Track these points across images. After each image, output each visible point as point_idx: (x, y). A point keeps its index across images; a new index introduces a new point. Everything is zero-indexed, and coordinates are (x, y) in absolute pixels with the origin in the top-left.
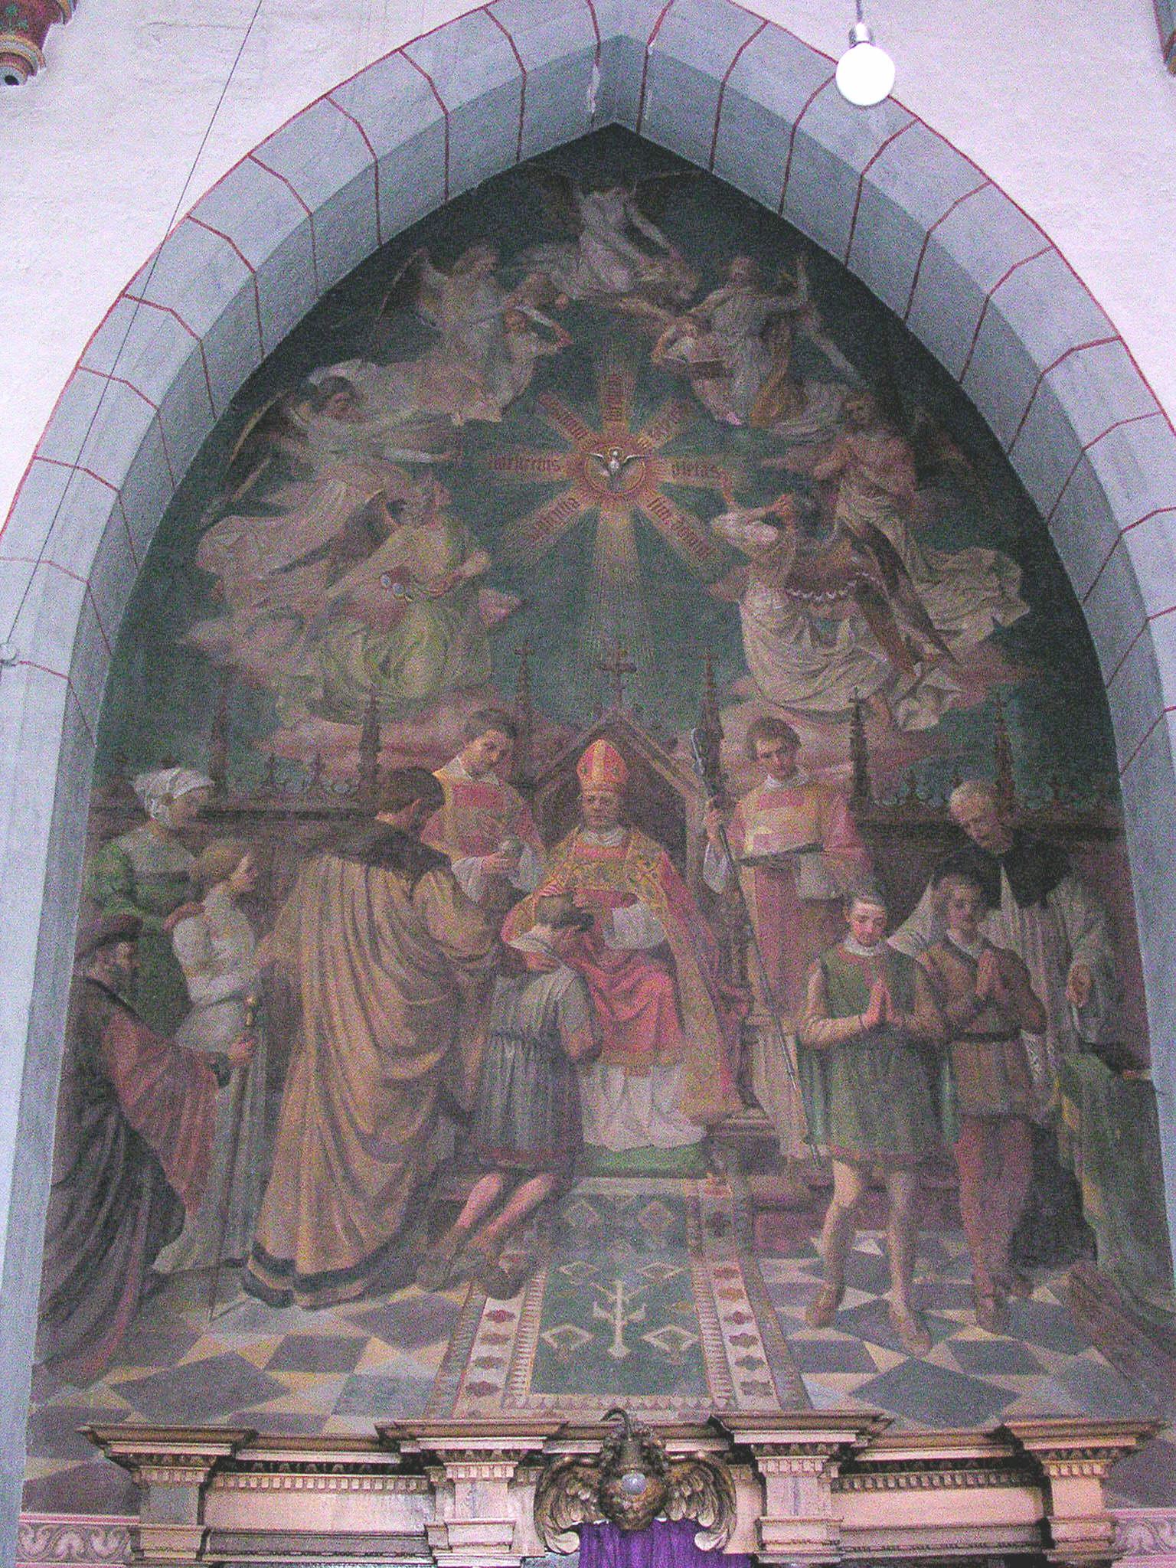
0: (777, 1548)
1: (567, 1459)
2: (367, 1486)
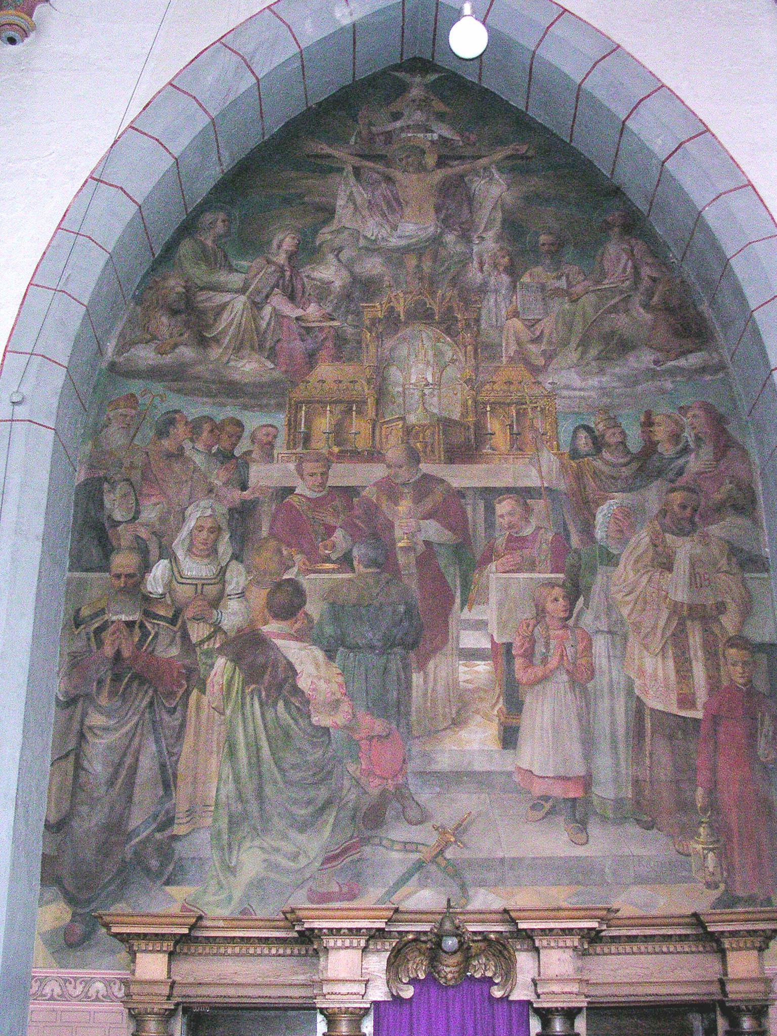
1: (411, 937)
2: (266, 951)
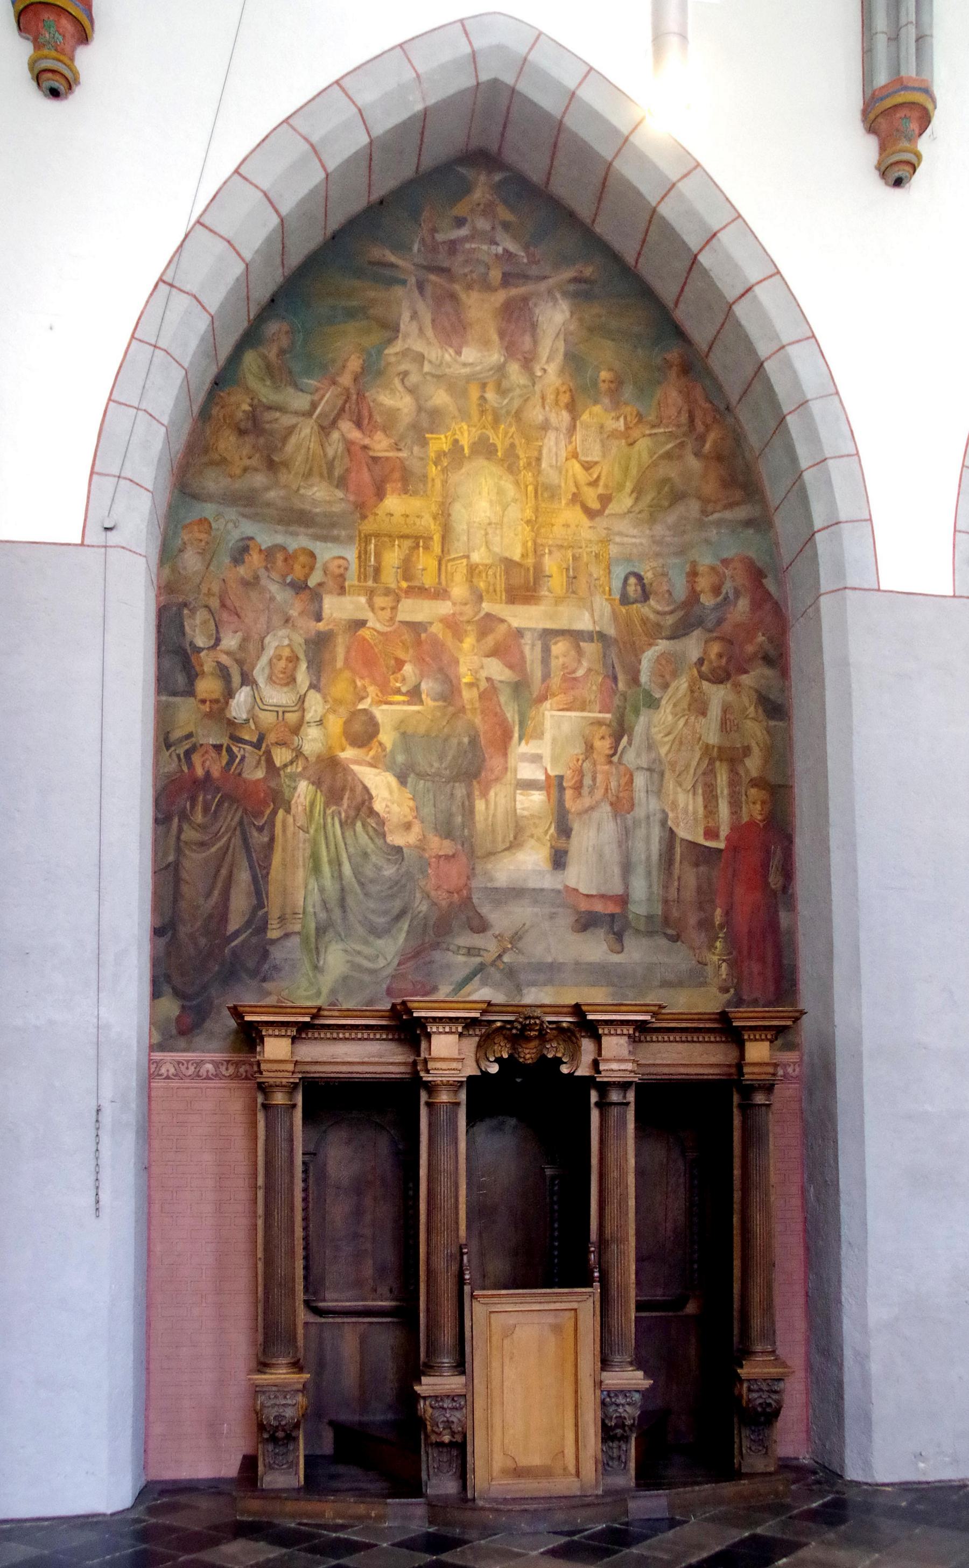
0: (608, 1074)
